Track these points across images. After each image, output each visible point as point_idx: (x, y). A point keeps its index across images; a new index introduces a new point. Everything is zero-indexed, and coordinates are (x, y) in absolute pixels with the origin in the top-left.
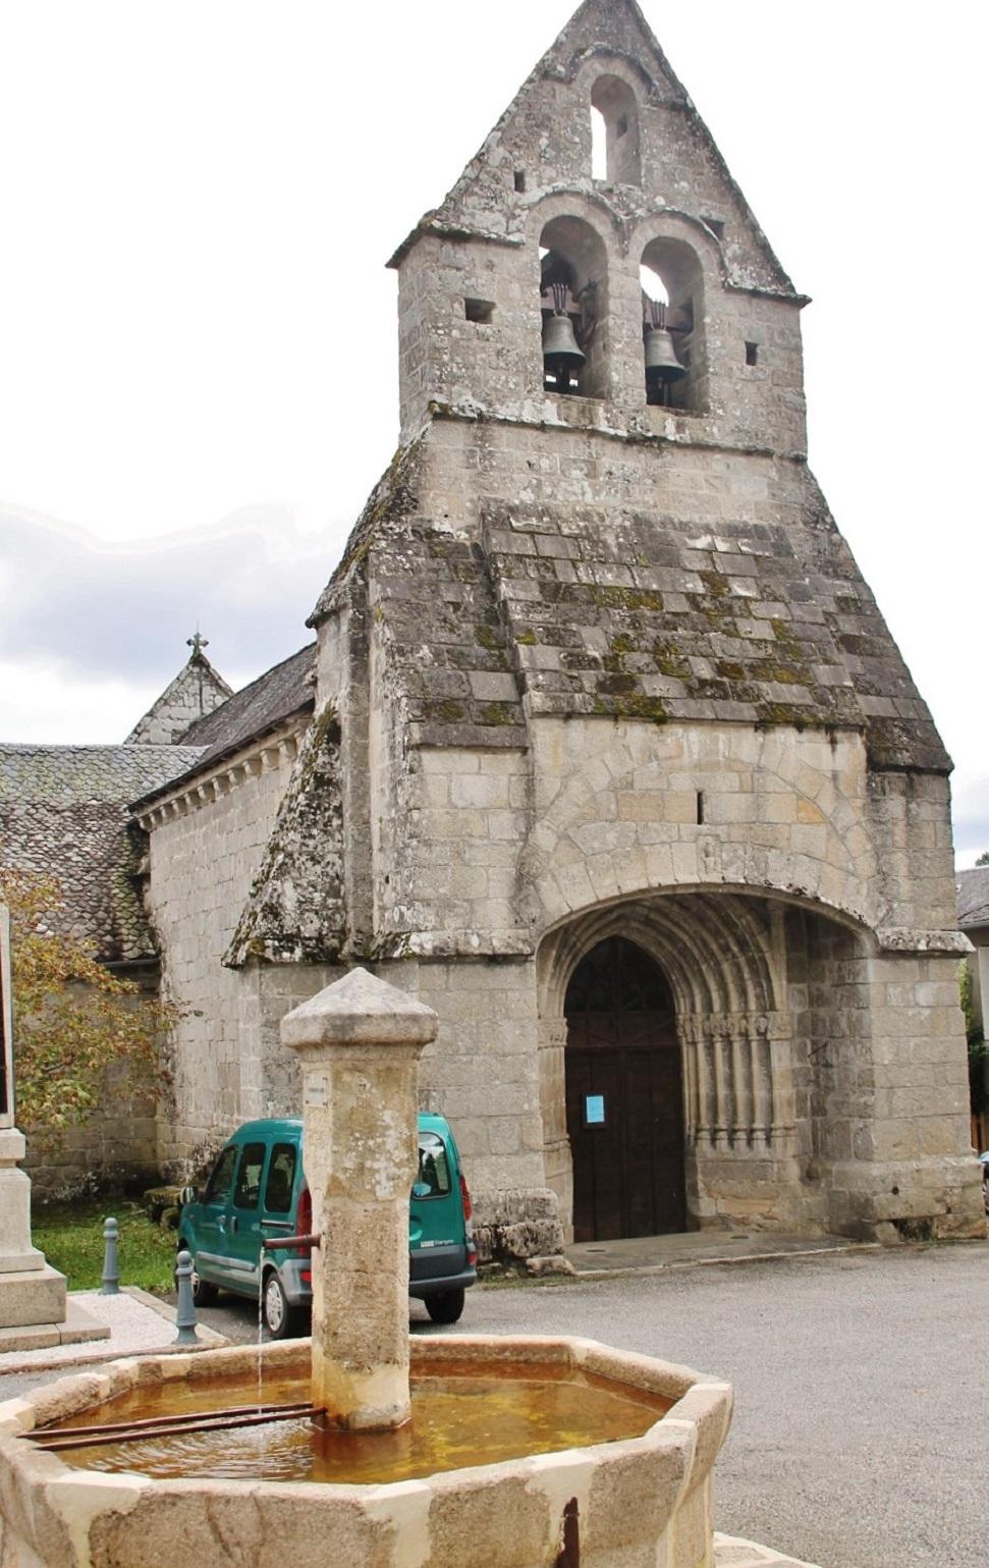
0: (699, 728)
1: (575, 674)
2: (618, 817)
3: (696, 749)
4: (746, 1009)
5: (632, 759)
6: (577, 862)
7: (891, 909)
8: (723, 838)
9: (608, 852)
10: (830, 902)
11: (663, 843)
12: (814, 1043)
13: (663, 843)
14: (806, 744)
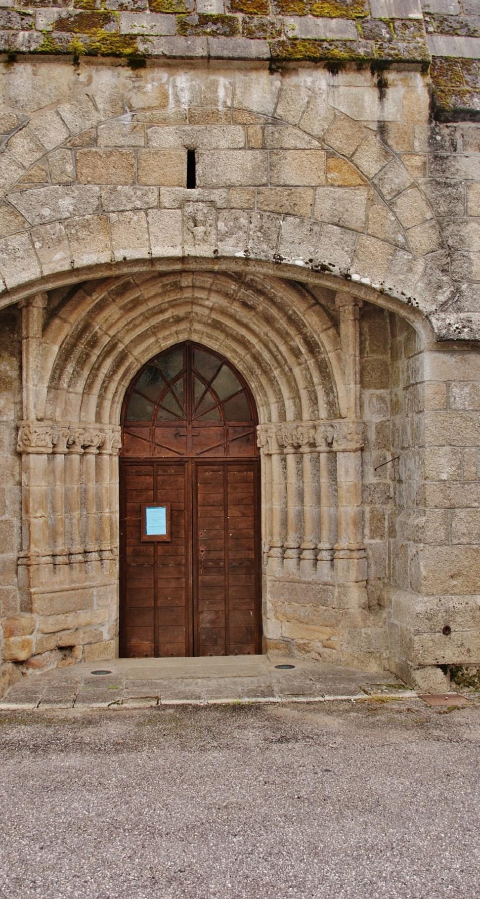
0: (192, 72)
1: (30, 11)
2: (76, 180)
3: (185, 97)
4: (315, 417)
5: (97, 109)
6: (22, 233)
7: (458, 290)
8: (220, 204)
9: (60, 221)
10: (366, 281)
11: (135, 210)
12: (392, 454)
13: (135, 210)
14: (342, 89)
